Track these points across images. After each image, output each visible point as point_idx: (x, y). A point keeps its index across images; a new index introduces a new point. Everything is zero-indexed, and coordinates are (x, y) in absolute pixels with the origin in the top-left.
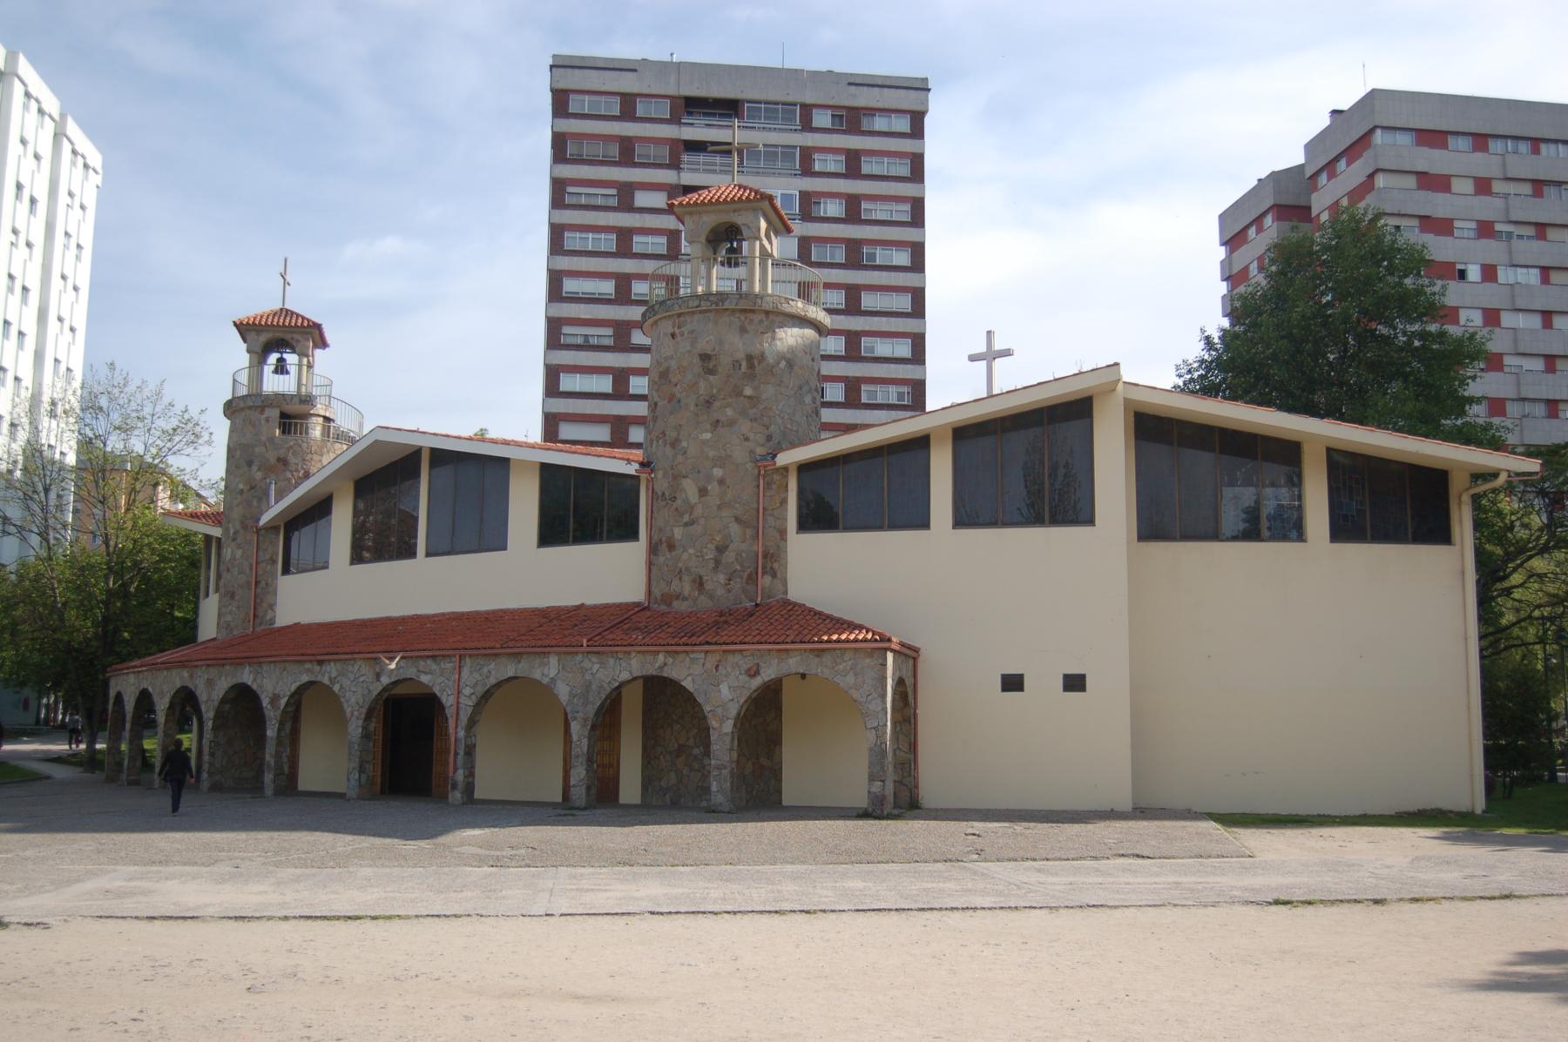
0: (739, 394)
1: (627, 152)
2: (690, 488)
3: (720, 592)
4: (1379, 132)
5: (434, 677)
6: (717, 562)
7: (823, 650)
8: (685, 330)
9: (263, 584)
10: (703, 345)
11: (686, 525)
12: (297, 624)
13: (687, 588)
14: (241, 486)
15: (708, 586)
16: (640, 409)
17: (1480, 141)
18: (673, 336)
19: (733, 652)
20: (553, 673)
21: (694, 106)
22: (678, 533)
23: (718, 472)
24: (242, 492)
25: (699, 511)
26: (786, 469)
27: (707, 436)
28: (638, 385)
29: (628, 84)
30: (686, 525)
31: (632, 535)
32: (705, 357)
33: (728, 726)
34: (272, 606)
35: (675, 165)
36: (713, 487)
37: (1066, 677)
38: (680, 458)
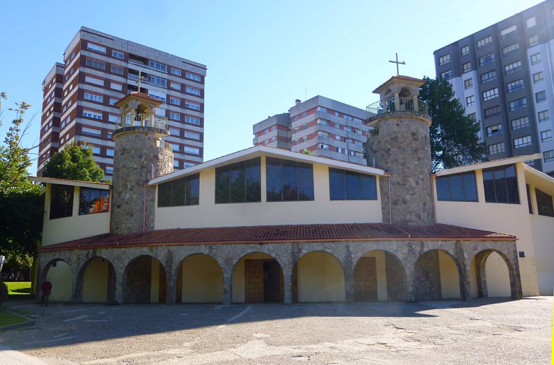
0: (424, 149)
1: (108, 68)
2: (412, 181)
3: (426, 220)
4: (319, 107)
5: (270, 249)
6: (424, 209)
7: (497, 241)
8: (404, 123)
9: (148, 210)
10: (413, 129)
11: (411, 195)
12: (179, 229)
13: (414, 218)
14: (135, 166)
15: (422, 218)
16: (111, 161)
17: (341, 114)
18: (398, 125)
19: (313, 242)
20: (395, 248)
21: (132, 57)
22: (408, 197)
23: (421, 176)
24: (136, 168)
25: (416, 190)
26: (153, 186)
27: (416, 163)
28: (110, 153)
29: (110, 44)
30: (411, 195)
31: (376, 199)
32: (413, 134)
33: (122, 271)
34: (153, 221)
35: (125, 77)
36: (420, 181)
37: (523, 252)
38: (406, 170)
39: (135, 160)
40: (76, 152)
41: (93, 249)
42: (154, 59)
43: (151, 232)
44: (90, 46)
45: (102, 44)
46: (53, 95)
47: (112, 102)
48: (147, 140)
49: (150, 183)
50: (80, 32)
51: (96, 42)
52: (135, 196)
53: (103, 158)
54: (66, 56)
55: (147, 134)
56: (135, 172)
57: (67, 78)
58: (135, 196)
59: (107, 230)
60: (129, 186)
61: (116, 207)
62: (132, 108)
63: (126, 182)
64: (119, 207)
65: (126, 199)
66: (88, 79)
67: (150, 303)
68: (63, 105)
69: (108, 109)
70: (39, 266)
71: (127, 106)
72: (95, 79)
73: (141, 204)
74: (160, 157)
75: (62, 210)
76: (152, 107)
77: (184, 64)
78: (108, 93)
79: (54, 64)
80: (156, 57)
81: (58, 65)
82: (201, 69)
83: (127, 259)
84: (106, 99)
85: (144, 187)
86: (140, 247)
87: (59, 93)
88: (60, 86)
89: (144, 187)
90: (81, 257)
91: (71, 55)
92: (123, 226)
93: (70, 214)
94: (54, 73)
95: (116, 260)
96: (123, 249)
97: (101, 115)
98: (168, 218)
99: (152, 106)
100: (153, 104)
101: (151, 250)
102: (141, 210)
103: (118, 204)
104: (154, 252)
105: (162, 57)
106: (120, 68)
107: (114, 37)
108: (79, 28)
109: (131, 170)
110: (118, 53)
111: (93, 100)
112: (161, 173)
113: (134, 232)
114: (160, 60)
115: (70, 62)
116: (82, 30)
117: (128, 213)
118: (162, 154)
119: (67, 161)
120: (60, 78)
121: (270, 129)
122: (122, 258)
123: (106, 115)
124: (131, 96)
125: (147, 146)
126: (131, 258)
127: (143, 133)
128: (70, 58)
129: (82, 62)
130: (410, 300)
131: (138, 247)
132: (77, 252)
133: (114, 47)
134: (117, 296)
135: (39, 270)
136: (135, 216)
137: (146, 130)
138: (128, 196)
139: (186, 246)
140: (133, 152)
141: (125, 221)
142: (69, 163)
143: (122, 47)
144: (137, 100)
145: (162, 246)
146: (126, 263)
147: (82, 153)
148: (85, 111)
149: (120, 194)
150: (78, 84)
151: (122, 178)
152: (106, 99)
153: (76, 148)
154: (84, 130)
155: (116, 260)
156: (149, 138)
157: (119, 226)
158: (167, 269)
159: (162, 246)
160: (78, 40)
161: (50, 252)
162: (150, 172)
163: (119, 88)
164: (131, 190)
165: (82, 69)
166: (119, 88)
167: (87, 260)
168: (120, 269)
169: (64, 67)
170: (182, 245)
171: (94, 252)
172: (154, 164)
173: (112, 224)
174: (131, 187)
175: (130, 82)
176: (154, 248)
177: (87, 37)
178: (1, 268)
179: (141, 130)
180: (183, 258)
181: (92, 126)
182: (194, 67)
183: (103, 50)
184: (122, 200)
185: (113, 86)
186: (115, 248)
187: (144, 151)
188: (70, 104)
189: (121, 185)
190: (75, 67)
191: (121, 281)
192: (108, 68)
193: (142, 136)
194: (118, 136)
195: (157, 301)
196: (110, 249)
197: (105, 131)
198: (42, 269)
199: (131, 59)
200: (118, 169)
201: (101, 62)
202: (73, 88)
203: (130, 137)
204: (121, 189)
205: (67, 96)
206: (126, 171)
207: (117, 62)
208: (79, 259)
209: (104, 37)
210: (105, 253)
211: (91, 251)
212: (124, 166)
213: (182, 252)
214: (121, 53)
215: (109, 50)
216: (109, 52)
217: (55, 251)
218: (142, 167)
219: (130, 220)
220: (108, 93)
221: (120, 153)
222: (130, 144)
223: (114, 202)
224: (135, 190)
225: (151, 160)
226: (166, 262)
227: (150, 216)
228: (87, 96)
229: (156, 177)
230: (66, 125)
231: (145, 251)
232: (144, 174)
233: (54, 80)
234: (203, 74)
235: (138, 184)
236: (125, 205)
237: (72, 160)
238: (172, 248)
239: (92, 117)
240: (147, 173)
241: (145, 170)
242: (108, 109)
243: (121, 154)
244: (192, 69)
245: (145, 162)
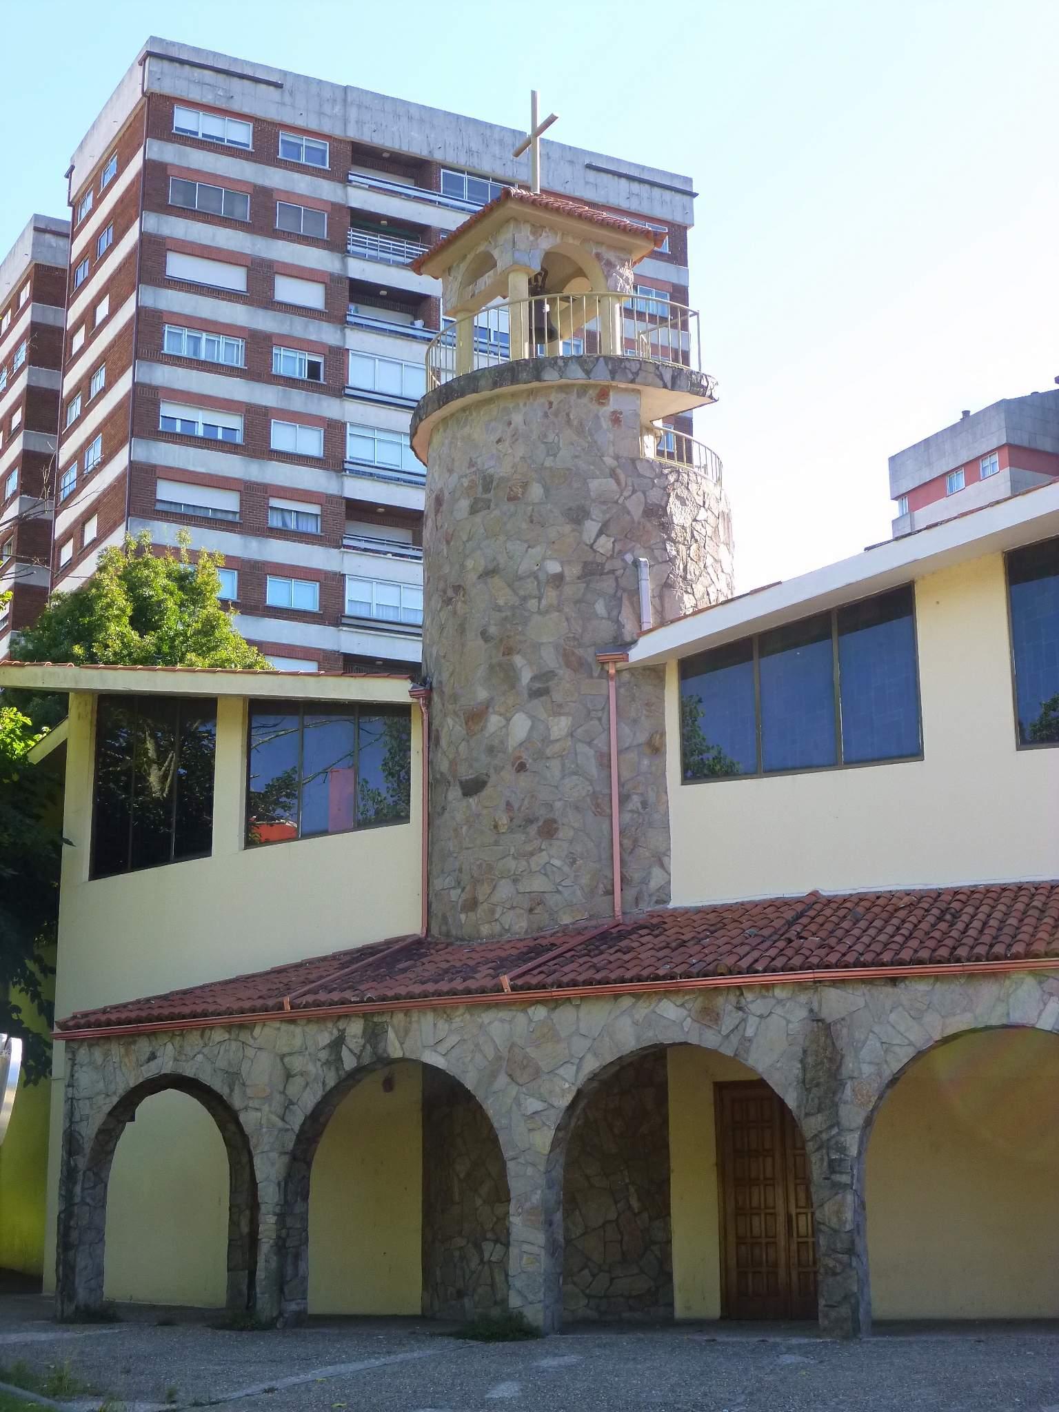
1: (263, 213)
14: (554, 567)
21: (365, 156)
24: (558, 579)
26: (653, 671)
29: (265, 105)
33: (543, 1140)
34: (661, 859)
35: (338, 246)
39: (552, 533)
40: (146, 583)
41: (366, 1016)
42: (462, 160)
43: (657, 924)
44: (184, 119)
45: (236, 106)
46: (22, 356)
47: (289, 363)
48: (605, 424)
49: (638, 654)
50: (142, 62)
51: (208, 99)
52: (560, 726)
53: (250, 620)
54: (79, 178)
55: (603, 395)
56: (551, 595)
57: (81, 274)
58: (560, 726)
59: (406, 921)
60: (526, 676)
61: (455, 793)
62: (516, 266)
63: (509, 651)
64: (473, 787)
65: (512, 743)
66: (178, 266)
67: (669, 1323)
68: (65, 393)
69: (266, 396)
70: (70, 1115)
71: (487, 262)
72: (205, 263)
73: (593, 770)
74: (679, 515)
75: (155, 827)
76: (610, 265)
77: (592, 175)
78: (264, 321)
79: (20, 223)
80: (470, 152)
81: (43, 228)
82: (668, 195)
83: (568, 1072)
84: (259, 348)
85: (605, 675)
86: (637, 996)
87: (48, 347)
88: (50, 315)
89: (605, 675)
90: (297, 1063)
91: (101, 168)
92: (505, 890)
93: (194, 839)
94: (22, 264)
95: (502, 1080)
96: (539, 1013)
97: (236, 422)
98: (742, 842)
99: (611, 256)
100: (612, 247)
101: (709, 1016)
102: (599, 804)
103: (466, 773)
104: (728, 1023)
105: (496, 149)
106: (314, 206)
107: (285, 74)
108: (137, 48)
109: (530, 586)
110: (304, 141)
111: (203, 356)
112: (689, 602)
113: (566, 920)
114: (486, 166)
115: (97, 202)
116: (149, 54)
117: (530, 821)
118: (683, 502)
119: (113, 628)
120: (50, 284)
121: (972, 468)
122: (532, 1067)
123: (258, 421)
124: (512, 206)
125: (609, 461)
126: (592, 1065)
127: (583, 390)
128: (96, 186)
129: (154, 190)
130: (70, 1227)
131: (627, 1002)
132: (274, 1038)
133: (287, 117)
134: (518, 1283)
135: (71, 1142)
136: (564, 833)
137: (601, 375)
138: (520, 726)
139: (922, 987)
140: (536, 491)
141: (512, 864)
142: (121, 636)
143: (321, 114)
144: (537, 229)
145: (768, 987)
146: (563, 1087)
147: (173, 586)
148: (167, 410)
149: (475, 717)
150: (134, 287)
151: (484, 635)
152: (259, 348)
153: (146, 565)
154: (167, 492)
155: (502, 1080)
156: (616, 419)
157: (483, 891)
158: (811, 1125)
159: (768, 987)
160: (132, 98)
161: (129, 1038)
162: (635, 593)
163: (312, 295)
164: (536, 694)
165: (156, 223)
166: (312, 295)
167: (331, 1083)
168: (529, 1129)
169: (68, 233)
170: (894, 981)
171: (374, 1035)
172: (650, 550)
173: (438, 884)
174: (534, 679)
175: (360, 270)
176: (725, 1004)
177: (173, 82)
178: (7, 1115)
179: (576, 374)
180: (904, 1054)
181: (198, 473)
182: (635, 187)
183: (241, 133)
184: (491, 750)
185: (287, 290)
186: (489, 1006)
187: (597, 485)
188: (99, 382)
189: (481, 672)
190: (118, 222)
191: (536, 1197)
192: (263, 213)
193: (581, 407)
194: (445, 420)
195: (712, 1307)
196: (461, 1018)
197: (255, 497)
198: (89, 1131)
199: (356, 170)
200: (458, 588)
201: (233, 187)
202: (113, 311)
203: (517, 418)
204: (482, 694)
205: (83, 350)
206: (504, 597)
207: (302, 184)
208: (289, 1075)
209: (242, 77)
210: (435, 1040)
211: (355, 1028)
212: (489, 573)
213: (893, 1024)
214: (317, 144)
215: (266, 132)
216: (267, 142)
217: (152, 1034)
218: (592, 571)
219: (543, 858)
220: (264, 321)
221: (464, 504)
222: (521, 450)
223: (444, 766)
224: (557, 696)
225: (630, 535)
226: (806, 1085)
227: (641, 834)
228: (176, 342)
229: (663, 621)
230: (83, 480)
231: (672, 1018)
232: (600, 608)
233: (25, 294)
234: (678, 218)
235: (578, 665)
236: (508, 774)
237: (135, 622)
238: (835, 1003)
239: (200, 431)
240: (615, 602)
241: (607, 585)
242: (266, 396)
243: (473, 511)
244: (630, 195)
245: (605, 545)
